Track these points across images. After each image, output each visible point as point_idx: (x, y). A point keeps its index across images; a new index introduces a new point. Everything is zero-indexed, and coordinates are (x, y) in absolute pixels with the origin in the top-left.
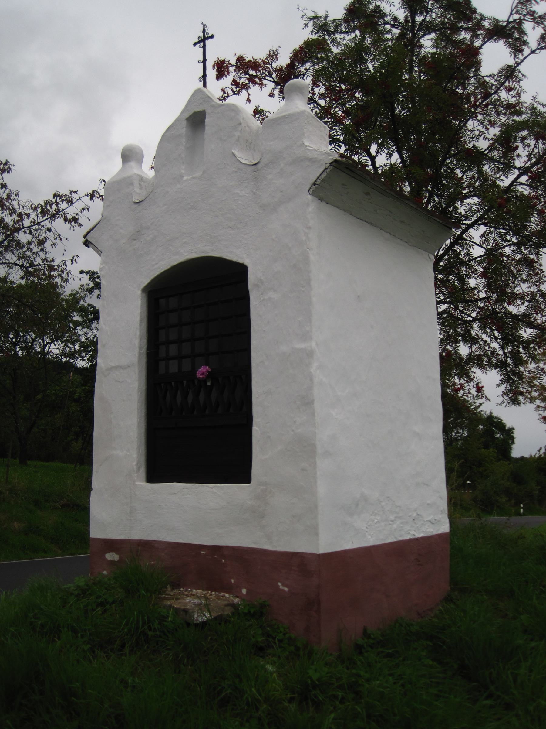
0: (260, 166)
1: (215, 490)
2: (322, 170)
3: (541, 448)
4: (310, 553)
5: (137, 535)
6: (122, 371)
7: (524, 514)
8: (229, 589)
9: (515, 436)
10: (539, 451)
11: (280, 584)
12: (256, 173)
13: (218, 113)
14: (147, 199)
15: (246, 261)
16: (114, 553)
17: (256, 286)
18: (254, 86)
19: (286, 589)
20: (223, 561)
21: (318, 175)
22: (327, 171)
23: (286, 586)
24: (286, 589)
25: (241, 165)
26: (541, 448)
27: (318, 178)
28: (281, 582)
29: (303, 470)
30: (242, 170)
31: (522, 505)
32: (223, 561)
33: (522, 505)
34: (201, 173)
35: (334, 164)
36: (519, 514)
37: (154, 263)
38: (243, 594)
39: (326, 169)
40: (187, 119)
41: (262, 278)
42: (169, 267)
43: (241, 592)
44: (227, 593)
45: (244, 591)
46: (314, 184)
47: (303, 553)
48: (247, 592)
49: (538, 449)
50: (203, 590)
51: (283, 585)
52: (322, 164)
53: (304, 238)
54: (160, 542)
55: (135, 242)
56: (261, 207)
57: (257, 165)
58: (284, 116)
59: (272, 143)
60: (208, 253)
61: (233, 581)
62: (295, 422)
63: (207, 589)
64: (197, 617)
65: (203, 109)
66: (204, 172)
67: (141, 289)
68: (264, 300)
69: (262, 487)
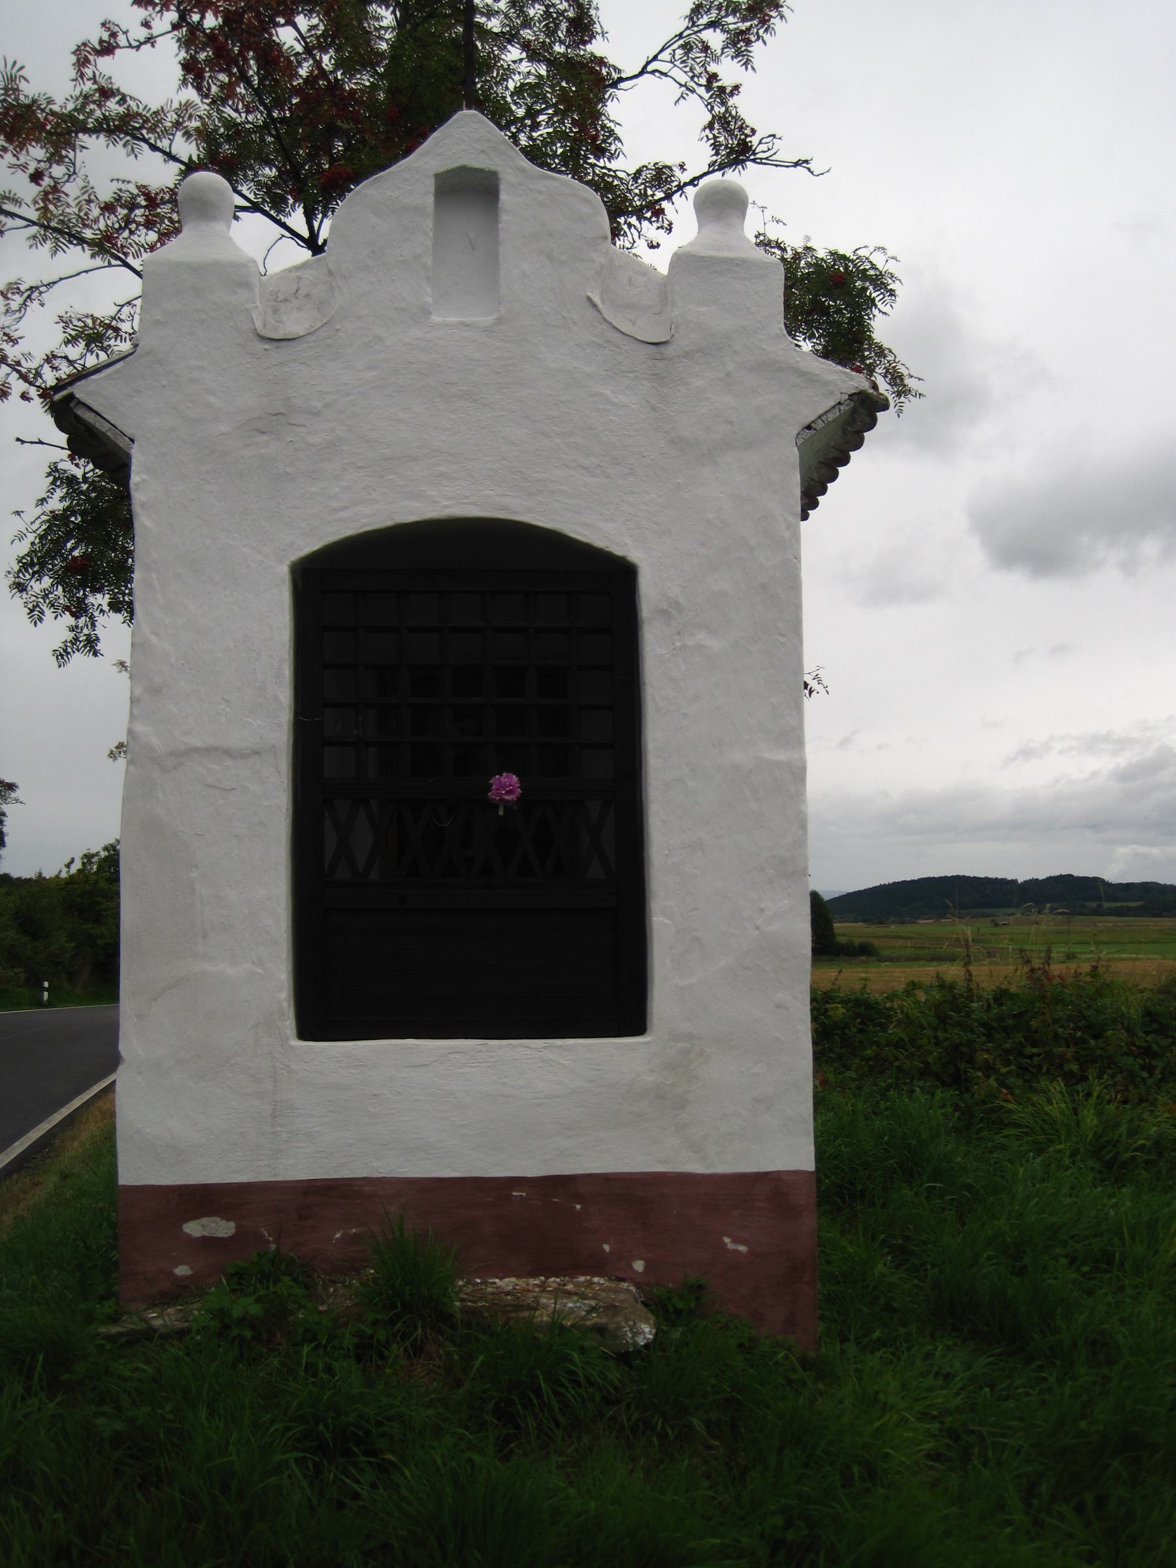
0: (669, 351)
1: (548, 1055)
2: (832, 403)
3: (73, 861)
4: (793, 1172)
5: (298, 1165)
6: (229, 762)
7: (50, 1004)
8: (598, 1266)
9: (5, 830)
10: (68, 866)
11: (727, 1240)
12: (660, 364)
13: (540, 192)
14: (313, 338)
15: (634, 555)
16: (218, 1219)
17: (665, 614)
18: (179, 40)
19: (742, 1248)
20: (578, 1207)
21: (821, 411)
22: (842, 408)
23: (743, 1242)
24: (742, 1248)
25: (615, 336)
26: (73, 861)
27: (820, 417)
28: (728, 1236)
29: (778, 1006)
30: (618, 347)
31: (46, 984)
32: (578, 1207)
33: (46, 984)
34: (489, 319)
35: (856, 398)
36: (40, 1004)
37: (335, 505)
38: (636, 1272)
39: (840, 403)
40: (437, 176)
41: (681, 600)
42: (389, 523)
43: (631, 1267)
44: (594, 1274)
45: (639, 1266)
46: (809, 427)
47: (778, 1172)
48: (646, 1267)
49: (67, 861)
50: (518, 1277)
51: (734, 1241)
52: (832, 392)
53: (787, 535)
54: (382, 1180)
55: (265, 438)
56: (672, 442)
57: (662, 348)
58: (732, 260)
59: (703, 309)
60: (516, 513)
61: (607, 1247)
62: (762, 910)
63: (533, 1274)
64: (633, 1338)
65: (493, 168)
66: (500, 320)
67: (288, 562)
68: (684, 646)
69: (679, 1045)
